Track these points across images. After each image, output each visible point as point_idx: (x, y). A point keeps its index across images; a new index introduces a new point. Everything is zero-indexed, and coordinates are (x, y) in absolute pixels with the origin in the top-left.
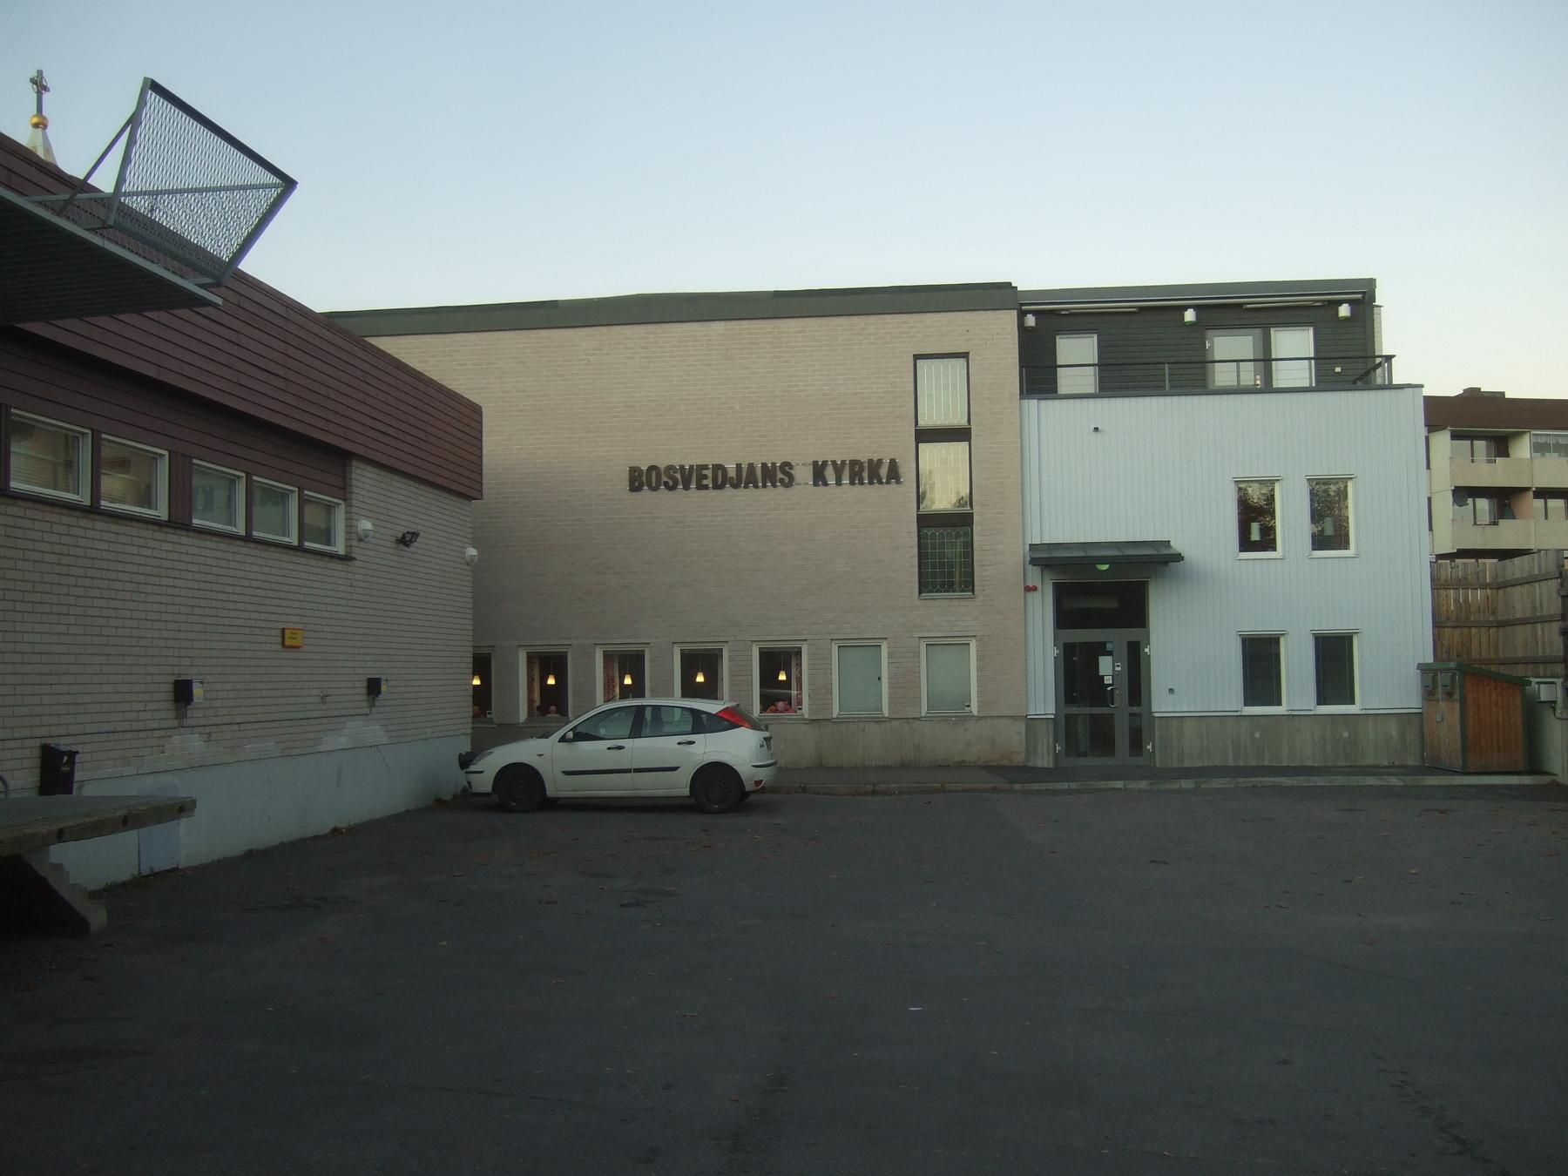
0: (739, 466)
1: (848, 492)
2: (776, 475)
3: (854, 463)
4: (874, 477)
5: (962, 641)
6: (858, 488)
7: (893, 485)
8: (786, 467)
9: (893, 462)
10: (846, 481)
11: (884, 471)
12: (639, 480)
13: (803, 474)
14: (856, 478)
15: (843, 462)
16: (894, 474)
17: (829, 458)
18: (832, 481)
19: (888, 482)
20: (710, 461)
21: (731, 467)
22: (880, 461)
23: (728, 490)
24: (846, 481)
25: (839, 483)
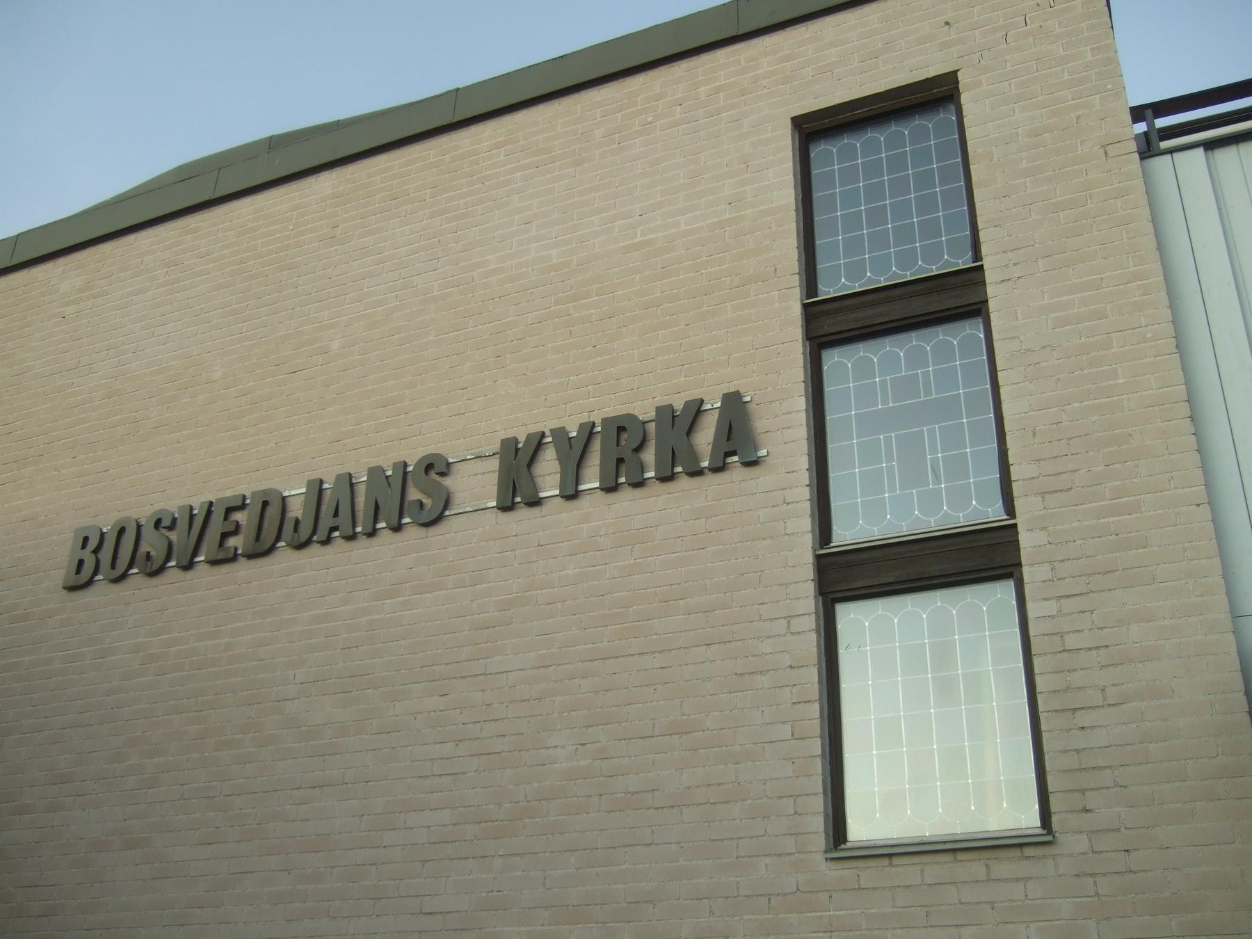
0: (317, 489)
1: (602, 513)
2: (408, 497)
3: (620, 427)
4: (678, 463)
5: (974, 307)
6: (627, 499)
7: (737, 474)
8: (435, 467)
9: (734, 404)
10: (591, 482)
11: (705, 437)
12: (115, 556)
13: (476, 484)
14: (623, 473)
15: (588, 432)
16: (738, 440)
17: (711, 482)
18: (550, 488)
19: (719, 468)
20: (247, 487)
21: (296, 491)
22: (696, 410)
23: (285, 557)
24: (591, 482)
25: (571, 495)
